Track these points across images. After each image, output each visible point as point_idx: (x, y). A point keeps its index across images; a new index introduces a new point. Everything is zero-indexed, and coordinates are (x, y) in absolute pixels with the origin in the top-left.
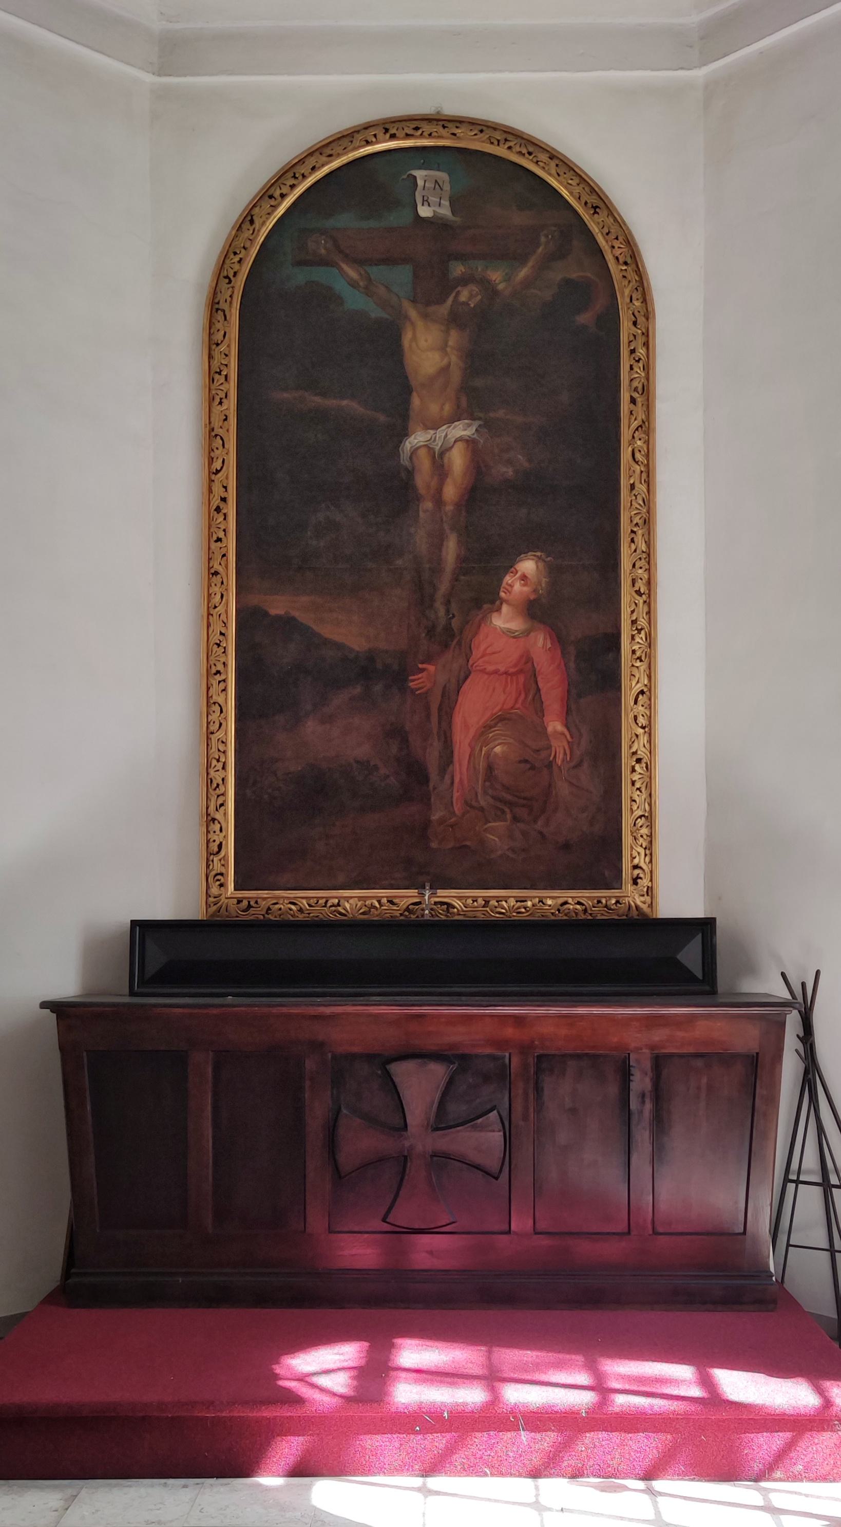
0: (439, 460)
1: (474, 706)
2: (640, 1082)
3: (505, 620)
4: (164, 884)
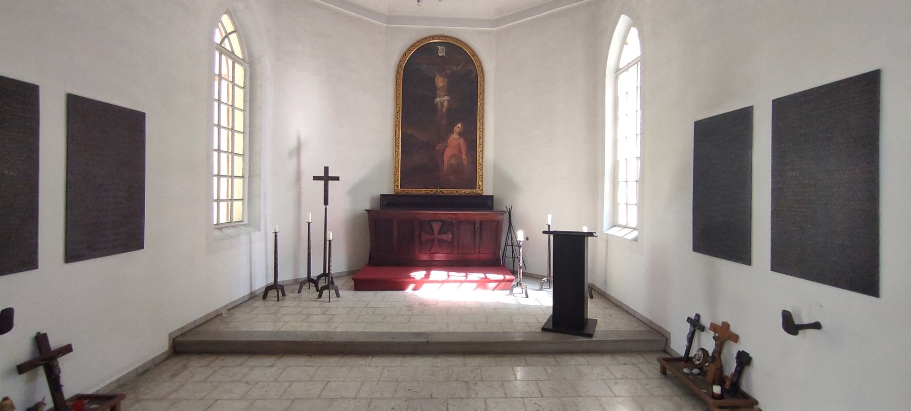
0: (442, 103)
1: (448, 153)
2: (477, 226)
3: (455, 136)
4: (387, 188)
